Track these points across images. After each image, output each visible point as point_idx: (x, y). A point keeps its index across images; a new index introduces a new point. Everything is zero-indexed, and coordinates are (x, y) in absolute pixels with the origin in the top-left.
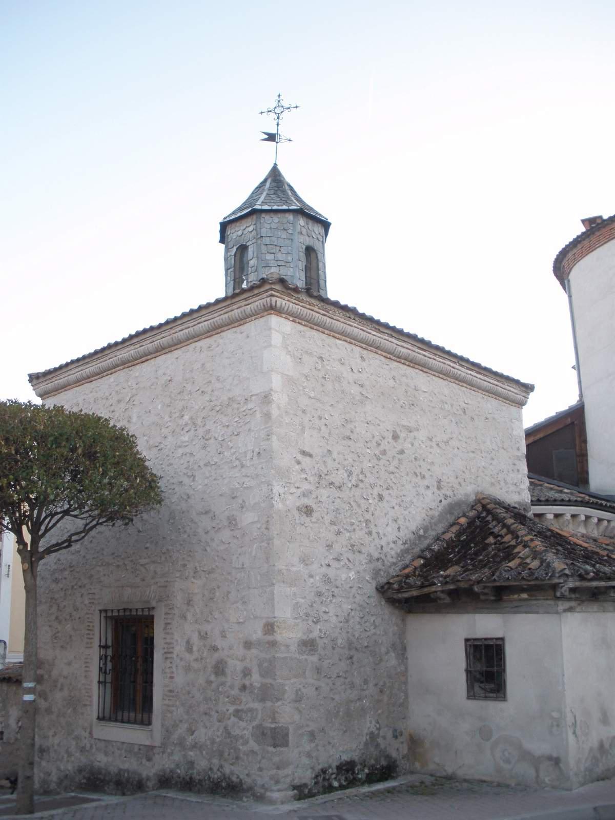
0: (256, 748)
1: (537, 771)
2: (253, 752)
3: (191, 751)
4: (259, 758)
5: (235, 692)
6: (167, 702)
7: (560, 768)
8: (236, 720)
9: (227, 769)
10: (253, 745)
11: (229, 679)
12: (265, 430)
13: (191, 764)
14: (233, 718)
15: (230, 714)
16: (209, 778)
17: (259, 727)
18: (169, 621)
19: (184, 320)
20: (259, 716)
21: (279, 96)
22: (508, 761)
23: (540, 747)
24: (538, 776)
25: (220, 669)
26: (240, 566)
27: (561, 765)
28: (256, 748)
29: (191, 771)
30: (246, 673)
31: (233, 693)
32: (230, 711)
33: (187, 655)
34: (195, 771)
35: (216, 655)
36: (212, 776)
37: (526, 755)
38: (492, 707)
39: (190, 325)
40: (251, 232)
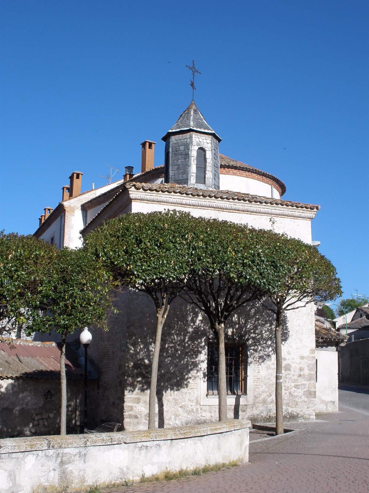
4: (308, 403)
5: (296, 377)
6: (255, 384)
7: (335, 405)
10: (304, 398)
11: (292, 372)
14: (293, 389)
15: (292, 387)
17: (308, 391)
21: (200, 73)
26: (298, 324)
27: (335, 404)
28: (306, 399)
29: (269, 414)
30: (301, 369)
31: (294, 378)
39: (270, 208)
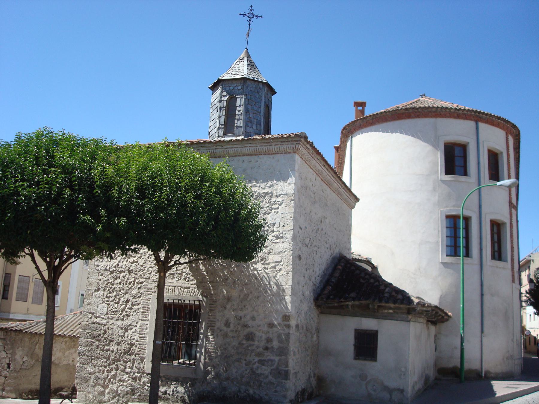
0: (274, 380)
1: (391, 396)
2: (271, 383)
3: (225, 381)
8: (260, 365)
9: (251, 392)
11: (256, 343)
12: (289, 214)
13: (225, 389)
14: (257, 364)
16: (238, 396)
18: (213, 309)
19: (235, 143)
20: (276, 364)
22: (375, 390)
23: (392, 384)
24: (391, 398)
25: (250, 337)
28: (274, 380)
30: (269, 340)
32: (255, 360)
33: (225, 329)
34: (227, 392)
35: (248, 330)
36: (239, 395)
37: (386, 388)
38: (369, 364)
40: (239, 90)
